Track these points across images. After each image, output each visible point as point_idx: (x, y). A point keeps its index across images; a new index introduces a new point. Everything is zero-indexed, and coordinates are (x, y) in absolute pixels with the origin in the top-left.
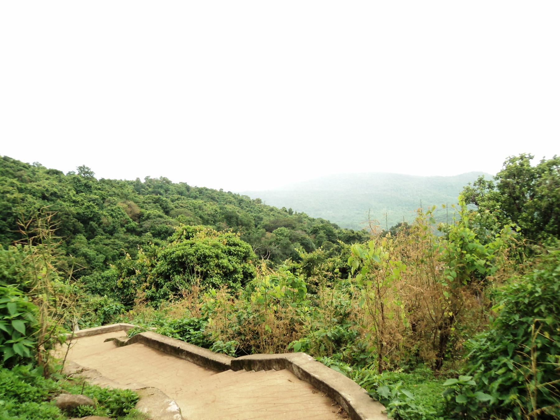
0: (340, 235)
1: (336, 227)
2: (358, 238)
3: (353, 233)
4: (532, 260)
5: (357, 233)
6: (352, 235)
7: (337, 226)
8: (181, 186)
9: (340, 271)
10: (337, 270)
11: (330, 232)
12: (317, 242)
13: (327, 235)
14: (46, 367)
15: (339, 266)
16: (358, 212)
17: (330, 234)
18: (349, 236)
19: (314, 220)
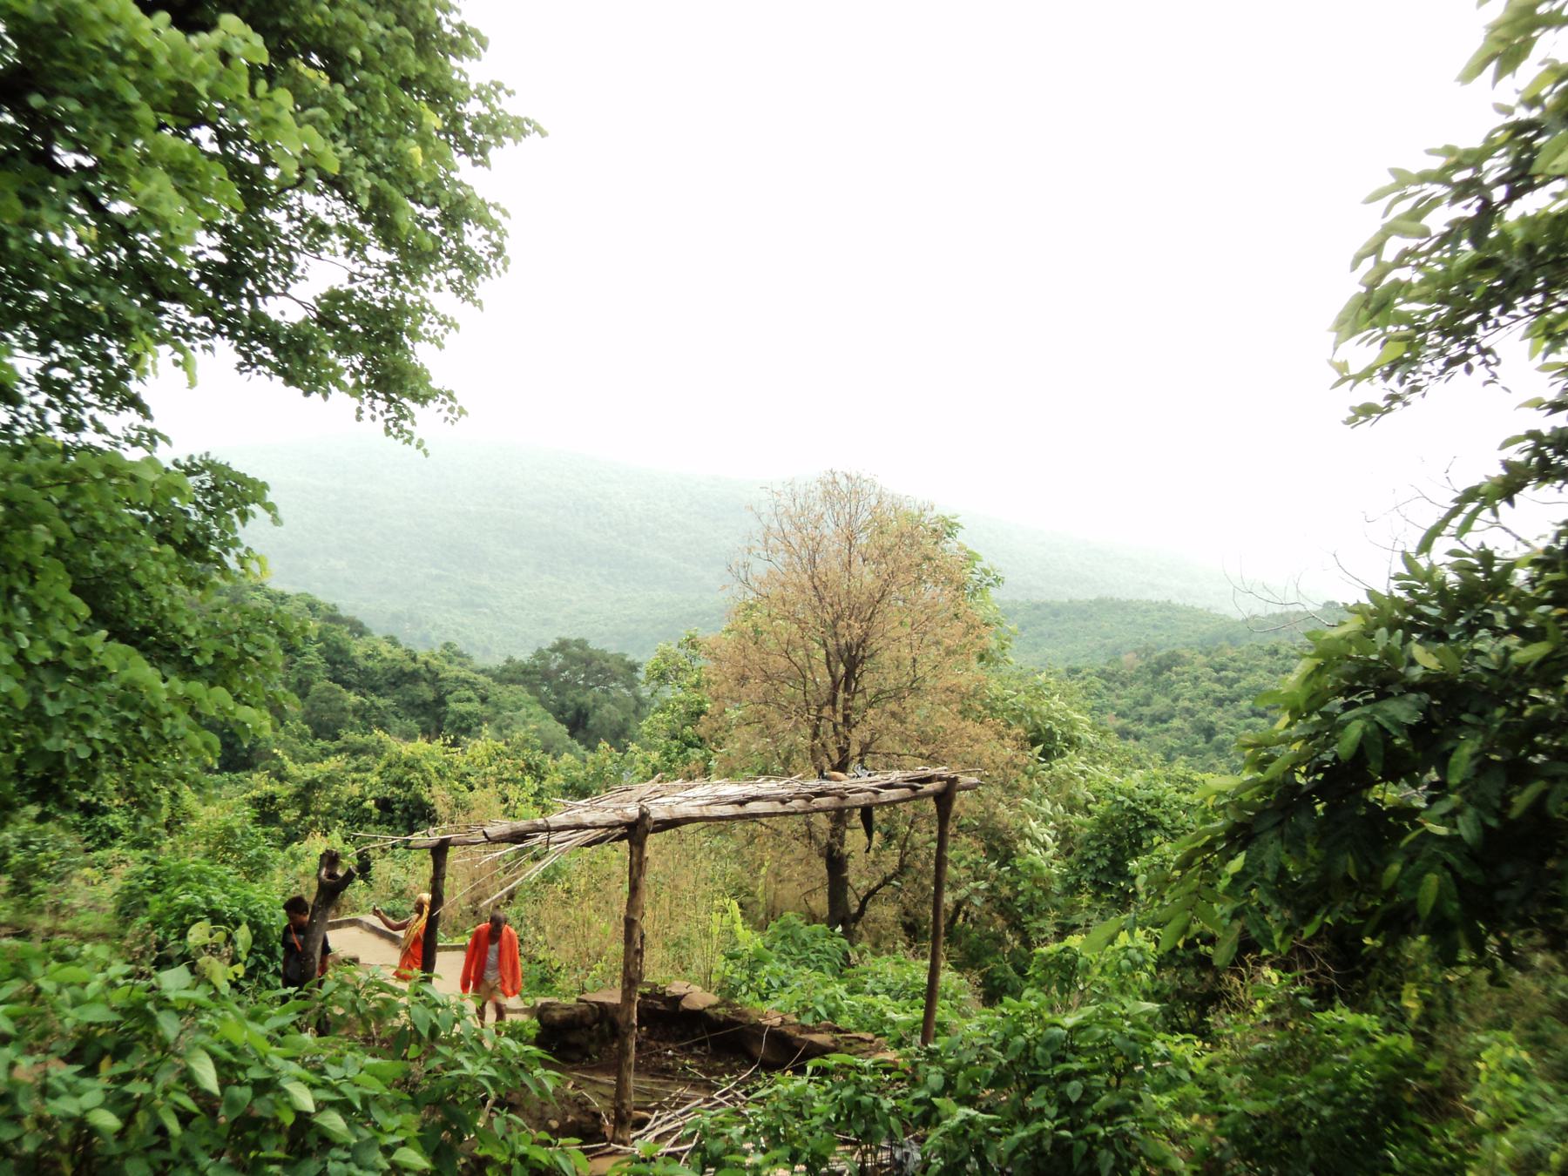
0: (370, 664)
1: (359, 629)
2: (428, 676)
3: (414, 659)
4: (1547, 101)
5: (426, 663)
6: (410, 666)
7: (361, 625)
8: (589, 1019)
9: (377, 805)
10: (369, 804)
11: (339, 650)
12: (293, 680)
13: (328, 660)
14: (1250, 1154)
15: (374, 793)
16: (435, 572)
17: (338, 658)
18: (401, 670)
19: (283, 598)
